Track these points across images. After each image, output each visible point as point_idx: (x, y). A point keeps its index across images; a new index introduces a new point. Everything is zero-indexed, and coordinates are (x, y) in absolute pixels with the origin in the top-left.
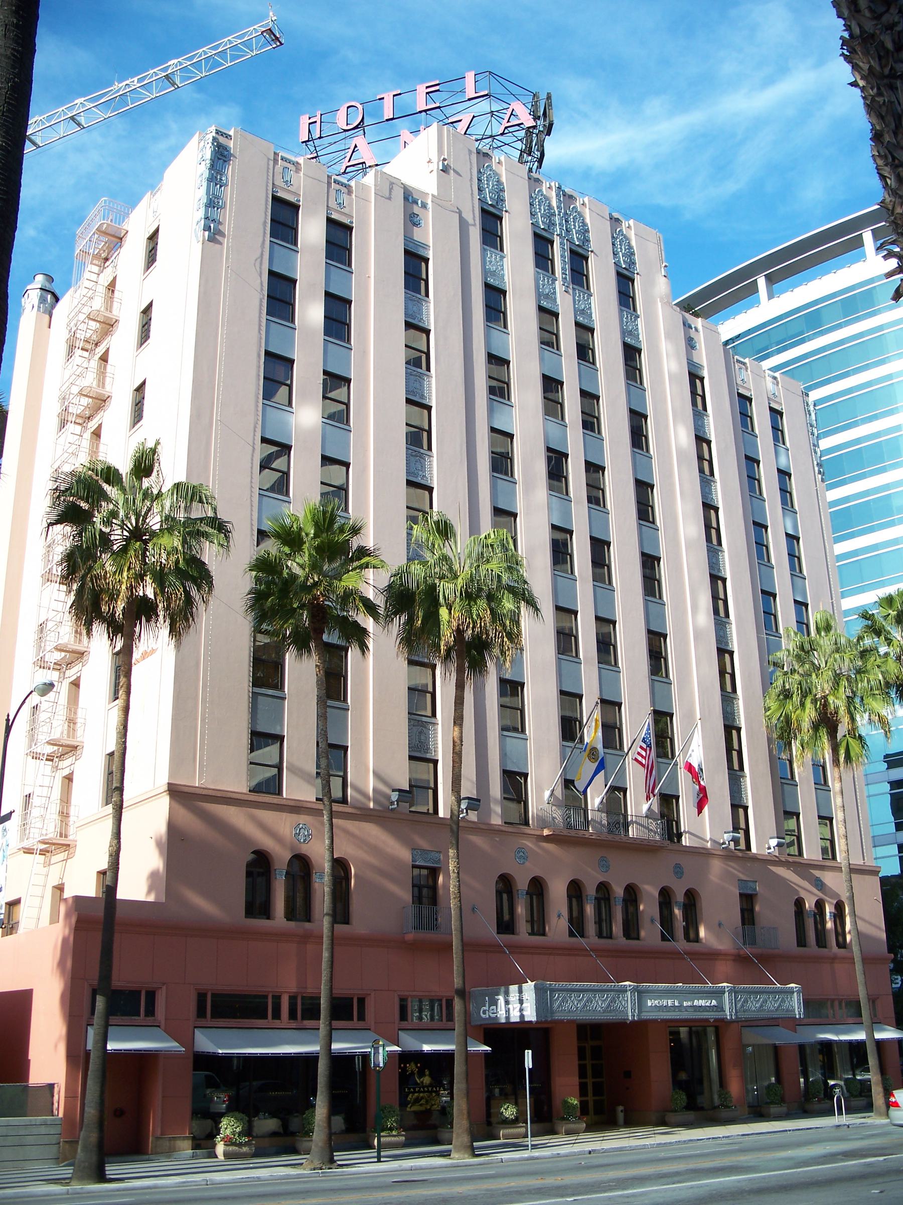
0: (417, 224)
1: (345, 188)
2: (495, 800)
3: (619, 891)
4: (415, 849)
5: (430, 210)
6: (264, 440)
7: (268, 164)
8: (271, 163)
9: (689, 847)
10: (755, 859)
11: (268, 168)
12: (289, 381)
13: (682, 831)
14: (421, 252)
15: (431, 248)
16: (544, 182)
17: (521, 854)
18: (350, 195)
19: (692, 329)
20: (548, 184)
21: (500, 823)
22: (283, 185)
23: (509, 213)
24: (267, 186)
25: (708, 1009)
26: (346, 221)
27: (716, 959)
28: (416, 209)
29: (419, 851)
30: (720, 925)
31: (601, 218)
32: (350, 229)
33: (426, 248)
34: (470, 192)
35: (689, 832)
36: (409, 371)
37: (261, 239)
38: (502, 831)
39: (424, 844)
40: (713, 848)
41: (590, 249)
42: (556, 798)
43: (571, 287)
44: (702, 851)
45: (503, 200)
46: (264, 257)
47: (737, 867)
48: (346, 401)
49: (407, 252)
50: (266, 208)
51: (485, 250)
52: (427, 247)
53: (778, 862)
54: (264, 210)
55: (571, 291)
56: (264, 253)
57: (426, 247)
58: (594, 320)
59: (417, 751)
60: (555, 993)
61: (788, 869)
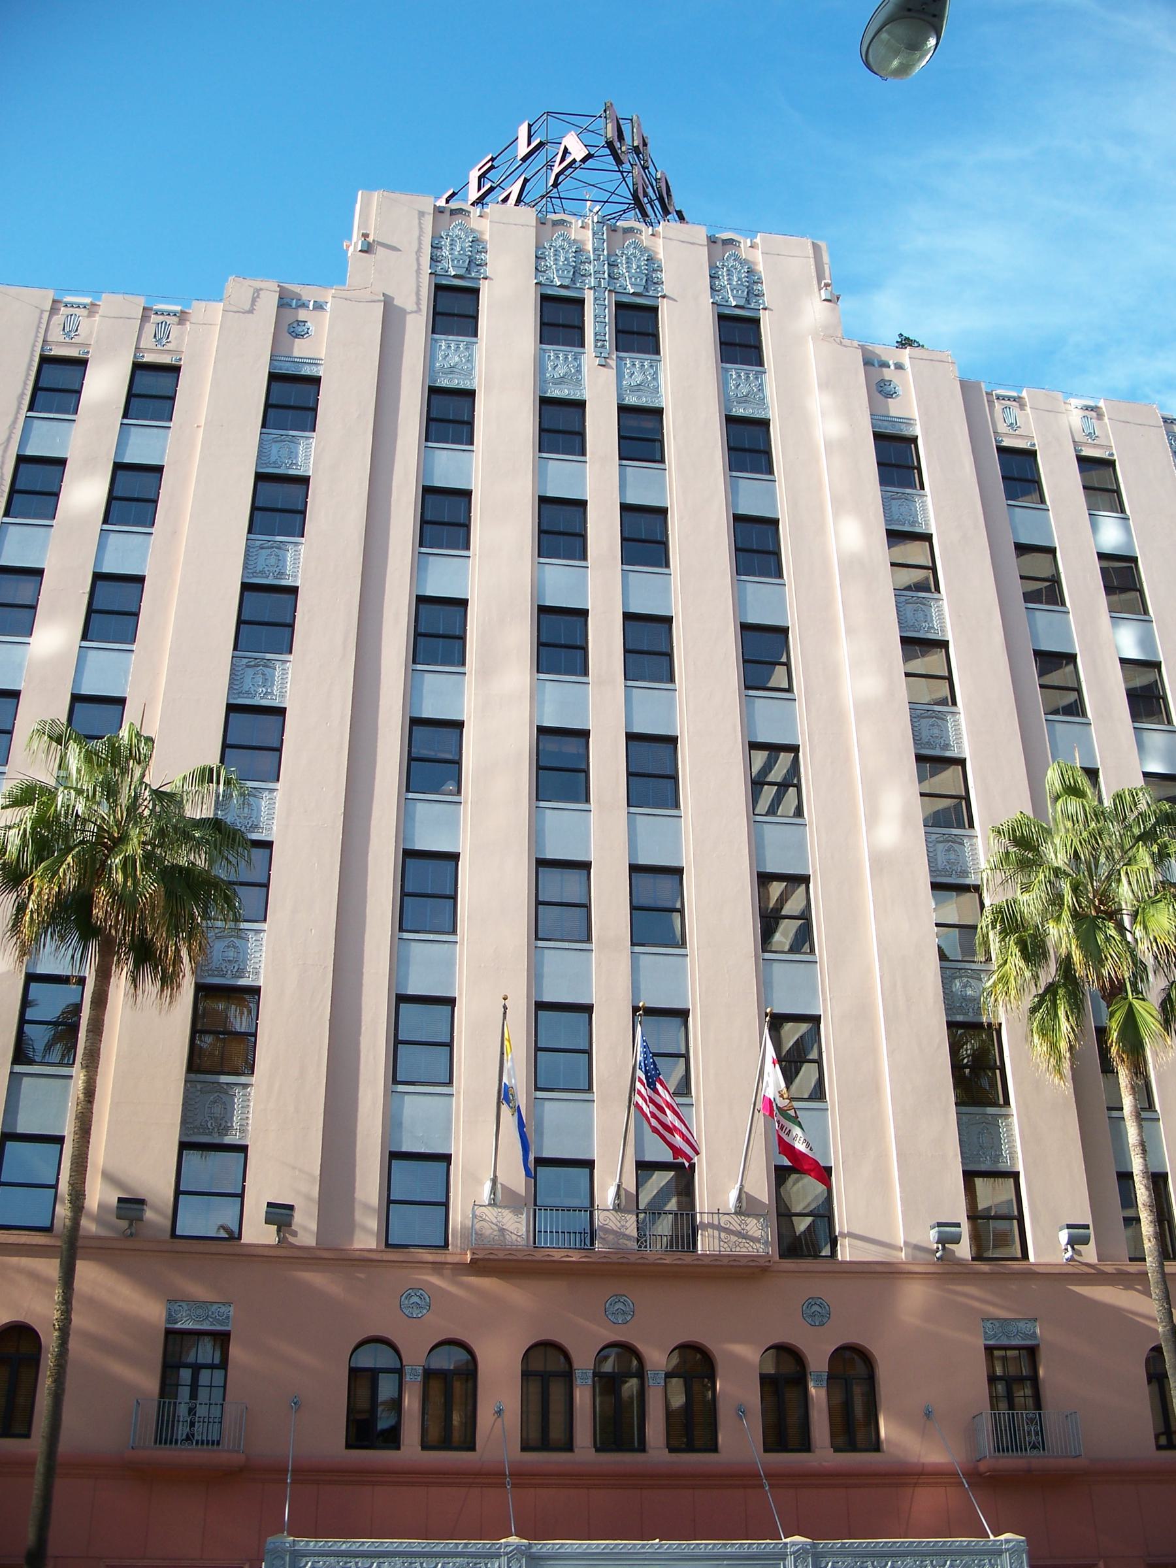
0: (890, 395)
1: (1092, 412)
2: (367, 1207)
4: (176, 1301)
5: (909, 370)
6: (754, 746)
7: (41, 318)
8: (46, 315)
9: (851, 1263)
10: (1032, 1275)
11: (40, 322)
12: (785, 656)
13: (837, 1234)
14: (906, 432)
15: (918, 422)
16: (742, 241)
17: (816, 1308)
18: (1103, 420)
19: (889, 367)
20: (748, 241)
21: (374, 1246)
22: (1085, 439)
23: (491, 279)
24: (34, 345)
26: (1105, 455)
27: (916, 1485)
28: (889, 374)
29: (995, 1322)
30: (928, 1414)
31: (689, 245)
32: (1032, 454)
33: (911, 424)
34: (415, 268)
35: (850, 1235)
36: (903, 599)
37: (11, 418)
38: (372, 1260)
39: (199, 1291)
40: (910, 1259)
41: (660, 294)
42: (509, 1192)
43: (614, 357)
44: (879, 1268)
45: (760, 295)
46: (12, 441)
47: (989, 1297)
48: (1076, 686)
49: (878, 437)
50: (28, 375)
51: (726, 370)
52: (912, 422)
53: (1096, 1276)
54: (23, 378)
55: (613, 363)
56: (13, 435)
57: (909, 422)
58: (768, 407)
59: (203, 1134)
60: (304, 1560)
61: (1127, 1288)
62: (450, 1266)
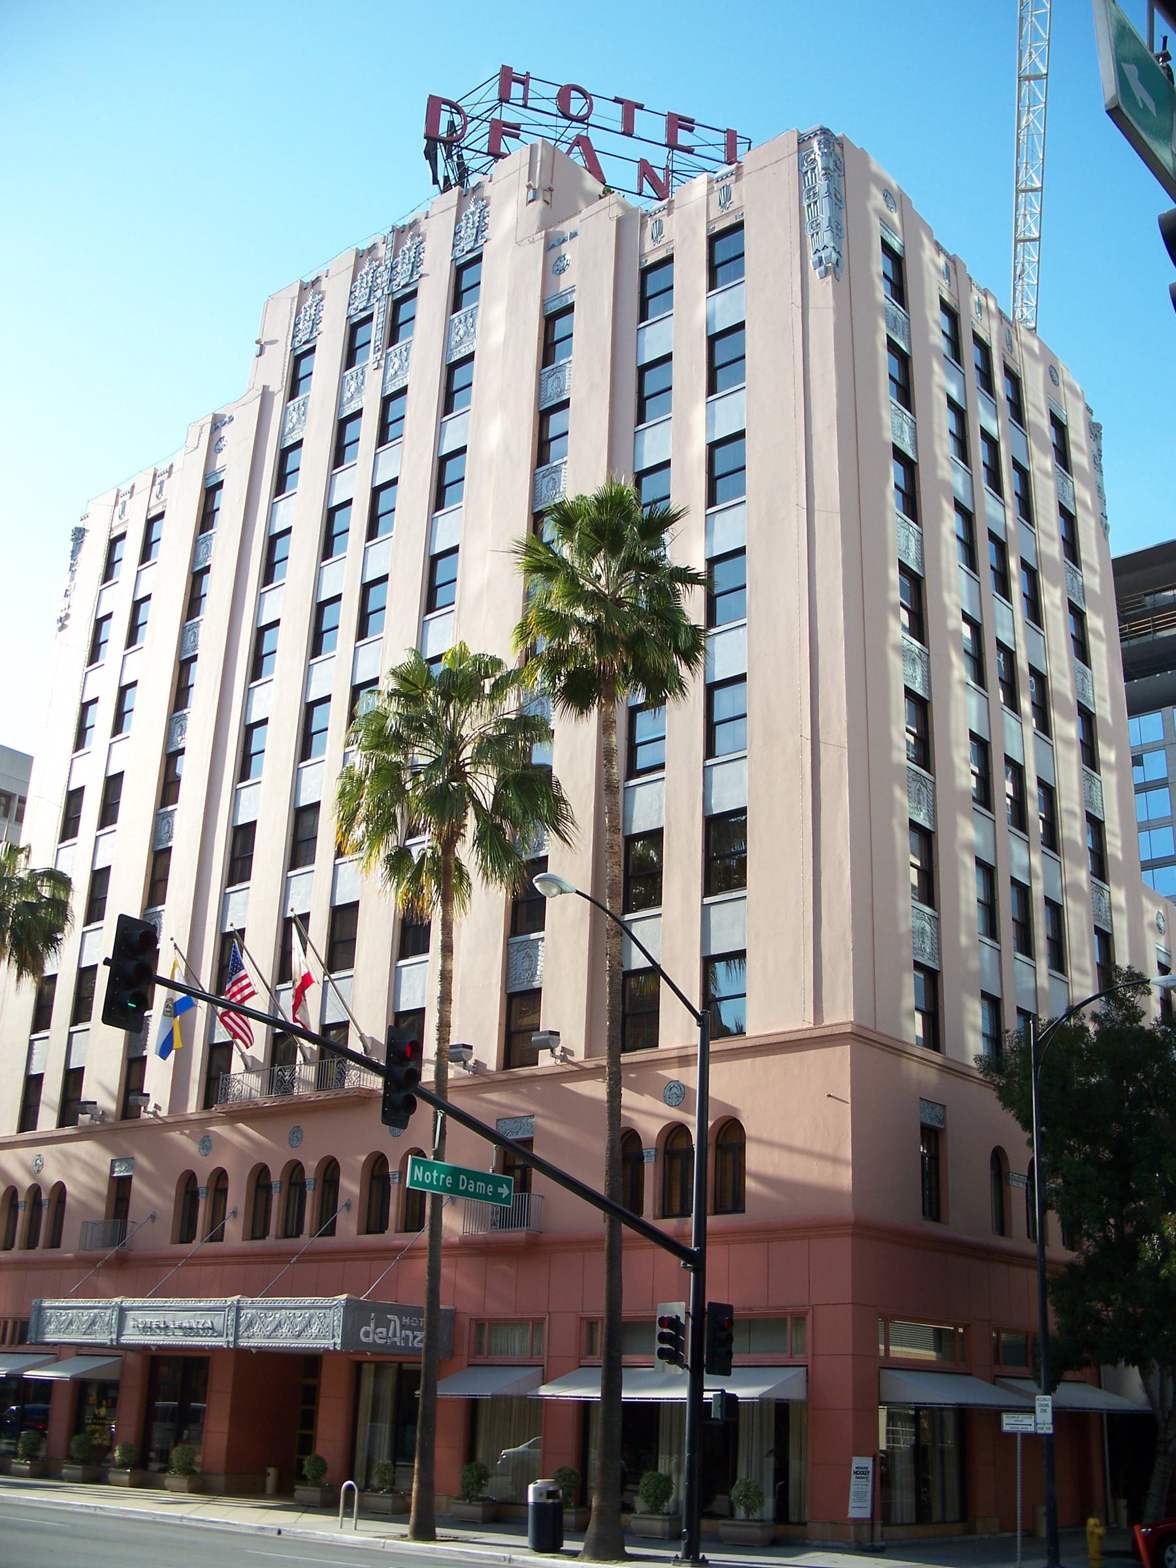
3: (311, 1166)
25: (201, 1332)
62: (676, 1059)
